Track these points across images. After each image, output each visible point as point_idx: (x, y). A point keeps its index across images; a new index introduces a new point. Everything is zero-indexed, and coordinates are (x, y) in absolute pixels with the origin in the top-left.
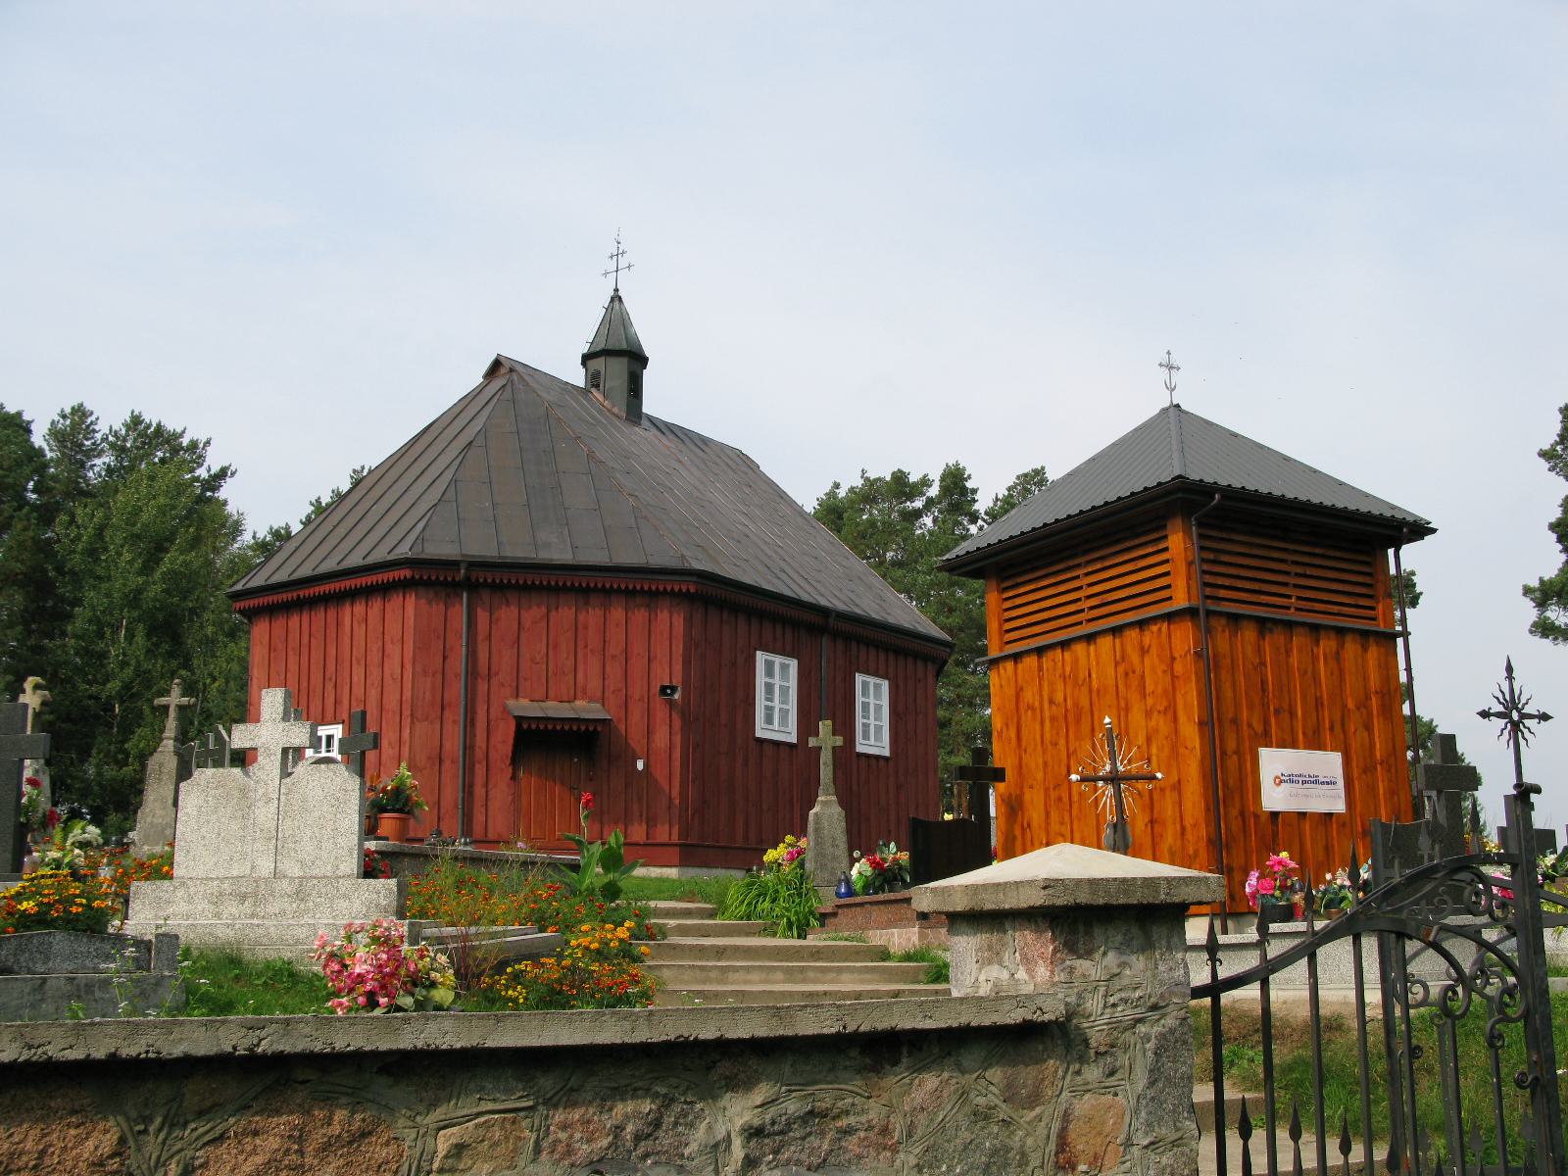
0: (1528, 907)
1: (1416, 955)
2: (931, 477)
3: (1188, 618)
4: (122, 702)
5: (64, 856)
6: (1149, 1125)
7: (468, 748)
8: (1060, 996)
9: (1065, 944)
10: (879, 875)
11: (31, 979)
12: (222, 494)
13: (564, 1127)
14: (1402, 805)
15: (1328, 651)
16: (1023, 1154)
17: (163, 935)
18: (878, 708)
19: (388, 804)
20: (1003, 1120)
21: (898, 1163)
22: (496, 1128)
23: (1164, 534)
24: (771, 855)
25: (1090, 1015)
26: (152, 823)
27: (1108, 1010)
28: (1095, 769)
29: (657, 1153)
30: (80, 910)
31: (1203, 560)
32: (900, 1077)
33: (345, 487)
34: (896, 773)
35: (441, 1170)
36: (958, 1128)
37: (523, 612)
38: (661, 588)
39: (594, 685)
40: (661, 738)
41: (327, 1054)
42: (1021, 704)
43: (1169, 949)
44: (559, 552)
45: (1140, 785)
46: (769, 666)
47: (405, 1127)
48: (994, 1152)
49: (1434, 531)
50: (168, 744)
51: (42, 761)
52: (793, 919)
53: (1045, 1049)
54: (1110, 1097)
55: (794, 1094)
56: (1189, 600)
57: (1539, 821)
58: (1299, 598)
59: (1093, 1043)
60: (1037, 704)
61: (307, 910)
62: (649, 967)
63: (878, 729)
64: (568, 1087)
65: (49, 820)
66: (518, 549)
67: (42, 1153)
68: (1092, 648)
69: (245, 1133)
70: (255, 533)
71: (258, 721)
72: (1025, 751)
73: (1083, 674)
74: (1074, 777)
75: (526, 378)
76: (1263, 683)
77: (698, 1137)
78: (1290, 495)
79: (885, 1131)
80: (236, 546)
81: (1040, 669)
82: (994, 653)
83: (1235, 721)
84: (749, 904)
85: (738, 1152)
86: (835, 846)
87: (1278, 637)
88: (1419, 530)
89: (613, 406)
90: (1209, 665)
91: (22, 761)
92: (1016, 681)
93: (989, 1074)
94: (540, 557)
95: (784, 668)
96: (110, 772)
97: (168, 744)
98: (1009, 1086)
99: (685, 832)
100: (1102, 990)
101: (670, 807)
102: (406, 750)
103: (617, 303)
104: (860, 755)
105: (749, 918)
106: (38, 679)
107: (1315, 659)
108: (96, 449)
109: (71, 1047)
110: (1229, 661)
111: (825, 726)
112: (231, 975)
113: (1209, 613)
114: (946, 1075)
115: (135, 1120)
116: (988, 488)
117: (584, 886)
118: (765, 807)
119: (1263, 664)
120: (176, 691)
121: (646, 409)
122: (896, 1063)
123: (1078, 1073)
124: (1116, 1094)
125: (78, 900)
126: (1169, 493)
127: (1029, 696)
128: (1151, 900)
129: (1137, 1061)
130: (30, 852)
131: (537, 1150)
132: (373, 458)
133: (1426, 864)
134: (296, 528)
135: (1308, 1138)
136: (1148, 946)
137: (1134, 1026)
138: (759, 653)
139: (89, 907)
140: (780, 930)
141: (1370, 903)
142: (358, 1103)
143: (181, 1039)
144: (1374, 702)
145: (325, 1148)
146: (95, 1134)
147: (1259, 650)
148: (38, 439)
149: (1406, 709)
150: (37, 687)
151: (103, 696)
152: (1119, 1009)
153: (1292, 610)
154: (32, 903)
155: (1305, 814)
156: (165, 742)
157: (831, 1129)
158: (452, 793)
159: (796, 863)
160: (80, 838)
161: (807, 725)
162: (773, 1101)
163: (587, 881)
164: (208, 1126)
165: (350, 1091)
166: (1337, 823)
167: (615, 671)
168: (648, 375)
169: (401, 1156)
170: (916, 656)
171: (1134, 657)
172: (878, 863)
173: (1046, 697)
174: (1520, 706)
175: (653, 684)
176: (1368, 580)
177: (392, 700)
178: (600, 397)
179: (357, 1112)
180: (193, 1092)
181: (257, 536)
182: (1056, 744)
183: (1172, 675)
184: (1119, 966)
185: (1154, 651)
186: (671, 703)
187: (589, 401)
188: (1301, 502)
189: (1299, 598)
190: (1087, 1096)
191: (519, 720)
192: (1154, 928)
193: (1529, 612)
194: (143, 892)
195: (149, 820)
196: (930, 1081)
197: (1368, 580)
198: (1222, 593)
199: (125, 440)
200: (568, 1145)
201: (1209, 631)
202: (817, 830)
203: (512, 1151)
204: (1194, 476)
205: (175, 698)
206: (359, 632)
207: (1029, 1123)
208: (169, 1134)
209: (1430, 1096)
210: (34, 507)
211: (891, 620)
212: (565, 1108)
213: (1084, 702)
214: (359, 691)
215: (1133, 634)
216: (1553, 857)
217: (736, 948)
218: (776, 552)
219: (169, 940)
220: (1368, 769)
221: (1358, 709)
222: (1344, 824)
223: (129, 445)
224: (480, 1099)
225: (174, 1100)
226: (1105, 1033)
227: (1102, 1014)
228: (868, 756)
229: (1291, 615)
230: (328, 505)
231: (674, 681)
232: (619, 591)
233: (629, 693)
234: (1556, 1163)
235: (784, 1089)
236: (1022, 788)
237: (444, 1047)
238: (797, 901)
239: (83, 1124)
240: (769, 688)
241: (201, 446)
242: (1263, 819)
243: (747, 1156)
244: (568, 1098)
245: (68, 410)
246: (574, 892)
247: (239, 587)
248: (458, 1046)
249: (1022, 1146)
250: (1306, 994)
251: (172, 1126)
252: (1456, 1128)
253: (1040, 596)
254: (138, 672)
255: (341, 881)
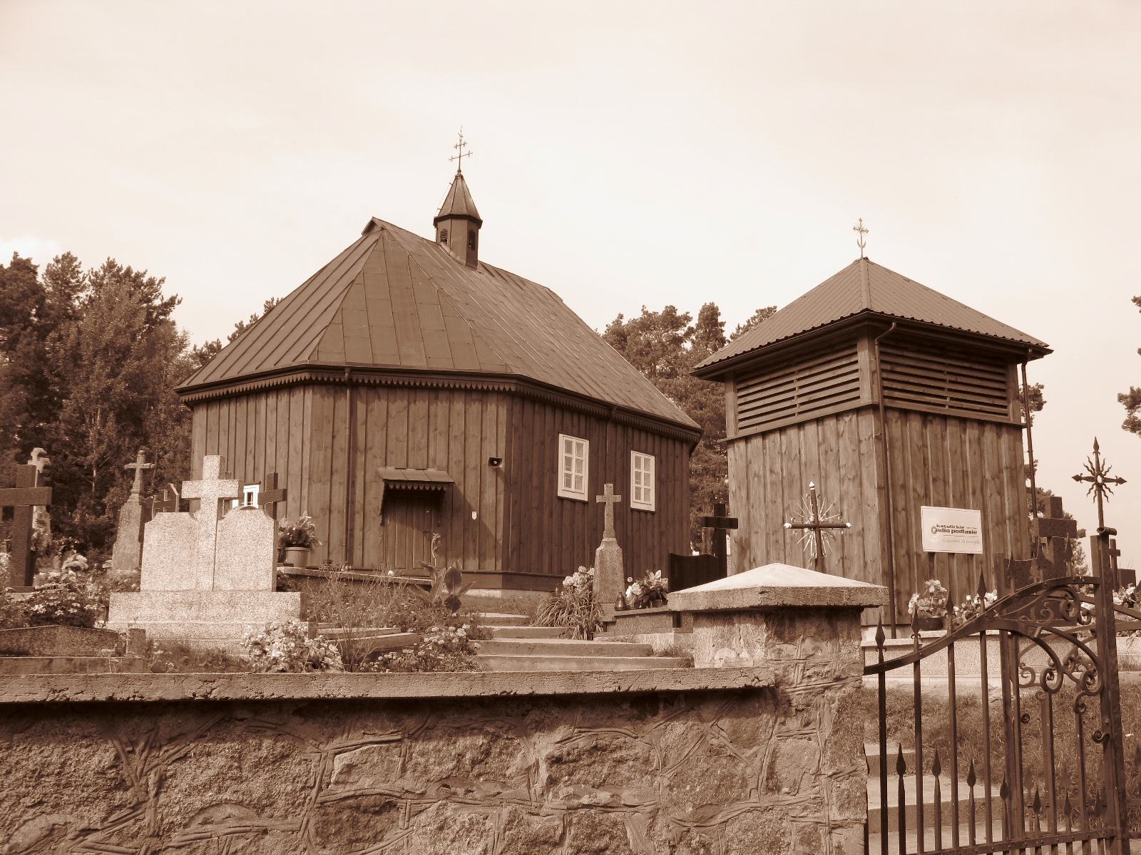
0: (1105, 615)
1: (1027, 650)
2: (690, 315)
3: (871, 411)
4: (98, 469)
5: (62, 575)
6: (833, 761)
7: (350, 502)
8: (771, 669)
9: (776, 633)
10: (646, 594)
11: (42, 660)
12: (172, 316)
13: (422, 754)
14: (1024, 551)
15: (972, 438)
16: (744, 779)
17: (134, 629)
18: (647, 476)
19: (293, 541)
20: (730, 756)
21: (656, 784)
22: (375, 754)
23: (855, 351)
24: (568, 581)
25: (792, 683)
26: (123, 554)
27: (806, 680)
28: (802, 519)
29: (488, 773)
30: (76, 611)
31: (883, 370)
32: (658, 724)
33: (260, 314)
34: (660, 525)
35: (337, 783)
36: (698, 760)
37: (390, 404)
38: (491, 388)
39: (441, 458)
40: (489, 496)
41: (258, 700)
42: (750, 472)
43: (849, 638)
44: (417, 362)
45: (835, 532)
46: (569, 445)
47: (311, 753)
48: (724, 778)
49: (1051, 351)
50: (135, 497)
51: (44, 508)
52: (584, 626)
53: (760, 707)
54: (806, 741)
55: (583, 734)
56: (872, 398)
57: (1123, 563)
58: (952, 399)
59: (794, 703)
60: (761, 473)
61: (236, 614)
62: (480, 658)
63: (647, 491)
64: (426, 726)
65: (49, 551)
66: (387, 359)
67: (63, 765)
68: (802, 433)
69: (201, 754)
70: (195, 347)
71: (200, 478)
72: (753, 507)
73: (795, 451)
74: (787, 525)
75: (395, 235)
76: (925, 459)
77: (516, 763)
78: (947, 324)
79: (647, 761)
80: (182, 355)
81: (764, 448)
82: (731, 435)
83: (904, 486)
84: (552, 615)
85: (544, 773)
86: (614, 573)
87: (934, 428)
88: (1040, 351)
89: (457, 255)
90: (886, 446)
91: (32, 506)
92: (747, 456)
93: (720, 723)
94: (403, 364)
95: (579, 446)
96: (91, 519)
97: (135, 497)
98: (734, 732)
99: (506, 564)
100: (801, 666)
101: (495, 546)
102: (305, 503)
103: (460, 180)
104: (633, 510)
105: (552, 625)
106: (42, 450)
107: (962, 442)
108: (79, 286)
109: (82, 692)
110: (900, 443)
111: (608, 488)
112: (182, 659)
113: (886, 408)
114: (690, 723)
115: (126, 743)
116: (731, 323)
117: (434, 600)
118: (564, 547)
119: (925, 446)
120: (140, 458)
121: (480, 258)
122: (655, 714)
123: (783, 723)
124: (810, 739)
125: (74, 604)
126: (858, 322)
127: (756, 467)
128: (837, 603)
129: (825, 717)
130: (38, 573)
131: (404, 770)
132: (282, 290)
133: (1035, 583)
134: (225, 343)
135: (945, 781)
136: (834, 636)
137: (823, 692)
138: (561, 436)
139: (82, 609)
140: (575, 633)
141: (992, 610)
142: (280, 735)
143: (157, 688)
144: (1005, 475)
145: (256, 765)
146: (99, 752)
147: (922, 436)
148: (40, 279)
149: (1028, 483)
150: (40, 455)
151: (86, 464)
152: (813, 679)
153: (947, 408)
154: (41, 606)
155: (953, 554)
156: (132, 495)
157: (609, 759)
158: (338, 534)
159: (586, 586)
160: (72, 564)
161: (595, 487)
162: (570, 738)
163: (437, 596)
164: (176, 749)
165: (274, 726)
166: (977, 560)
167: (456, 448)
168: (482, 233)
169: (309, 772)
170: (675, 439)
171: (832, 439)
172: (645, 586)
173: (768, 468)
174: (1103, 473)
175: (484, 457)
176: (1002, 386)
177: (295, 468)
178: (447, 249)
179: (279, 741)
180: (166, 725)
181: (197, 348)
182: (775, 502)
183: (859, 453)
184: (813, 649)
185: (846, 435)
186: (497, 472)
187: (439, 252)
188: (936, 326)
189: (952, 399)
190: (790, 739)
191: (387, 482)
192: (839, 623)
193: (1122, 413)
194: (118, 600)
195: (121, 551)
196: (679, 727)
197: (1002, 386)
198: (897, 394)
199: (103, 278)
200: (425, 767)
201: (886, 421)
202: (601, 563)
203: (386, 770)
204: (877, 309)
205: (140, 464)
206: (272, 418)
207: (748, 758)
208: (149, 753)
209: (1033, 752)
210: (36, 328)
211: (657, 413)
212: (423, 741)
213: (796, 472)
214: (271, 460)
215: (831, 423)
216: (1133, 588)
217: (543, 646)
218: (575, 363)
219: (138, 633)
220: (1000, 523)
221: (993, 479)
222: (981, 562)
223: (105, 282)
224: (364, 734)
225: (152, 730)
226: (803, 696)
227: (801, 683)
228: (639, 511)
229: (946, 411)
230: (248, 327)
231: (499, 454)
232: (460, 389)
233: (467, 464)
234: (1119, 794)
235: (576, 730)
236: (750, 533)
237: (339, 697)
238: (587, 613)
239: (90, 745)
240: (568, 461)
241: (157, 283)
242: (923, 557)
243: (550, 777)
244: (424, 733)
245: (60, 257)
246: (427, 604)
247: (184, 385)
248: (349, 696)
249: (743, 774)
250: (946, 681)
251: (152, 748)
252: (1050, 774)
253: (765, 395)
254: (110, 447)
255: (260, 593)
